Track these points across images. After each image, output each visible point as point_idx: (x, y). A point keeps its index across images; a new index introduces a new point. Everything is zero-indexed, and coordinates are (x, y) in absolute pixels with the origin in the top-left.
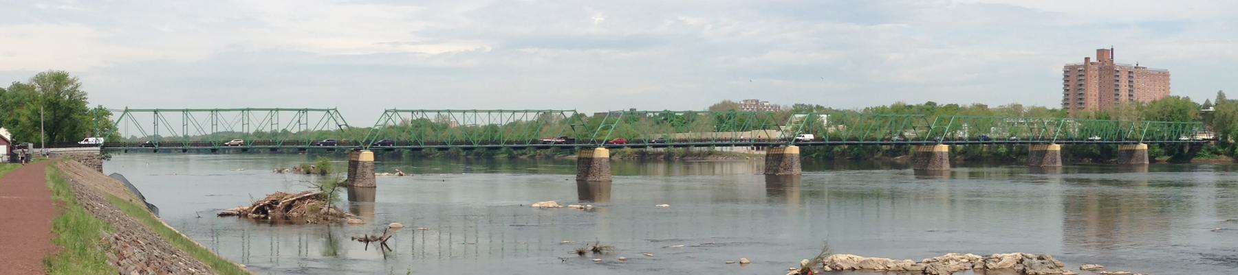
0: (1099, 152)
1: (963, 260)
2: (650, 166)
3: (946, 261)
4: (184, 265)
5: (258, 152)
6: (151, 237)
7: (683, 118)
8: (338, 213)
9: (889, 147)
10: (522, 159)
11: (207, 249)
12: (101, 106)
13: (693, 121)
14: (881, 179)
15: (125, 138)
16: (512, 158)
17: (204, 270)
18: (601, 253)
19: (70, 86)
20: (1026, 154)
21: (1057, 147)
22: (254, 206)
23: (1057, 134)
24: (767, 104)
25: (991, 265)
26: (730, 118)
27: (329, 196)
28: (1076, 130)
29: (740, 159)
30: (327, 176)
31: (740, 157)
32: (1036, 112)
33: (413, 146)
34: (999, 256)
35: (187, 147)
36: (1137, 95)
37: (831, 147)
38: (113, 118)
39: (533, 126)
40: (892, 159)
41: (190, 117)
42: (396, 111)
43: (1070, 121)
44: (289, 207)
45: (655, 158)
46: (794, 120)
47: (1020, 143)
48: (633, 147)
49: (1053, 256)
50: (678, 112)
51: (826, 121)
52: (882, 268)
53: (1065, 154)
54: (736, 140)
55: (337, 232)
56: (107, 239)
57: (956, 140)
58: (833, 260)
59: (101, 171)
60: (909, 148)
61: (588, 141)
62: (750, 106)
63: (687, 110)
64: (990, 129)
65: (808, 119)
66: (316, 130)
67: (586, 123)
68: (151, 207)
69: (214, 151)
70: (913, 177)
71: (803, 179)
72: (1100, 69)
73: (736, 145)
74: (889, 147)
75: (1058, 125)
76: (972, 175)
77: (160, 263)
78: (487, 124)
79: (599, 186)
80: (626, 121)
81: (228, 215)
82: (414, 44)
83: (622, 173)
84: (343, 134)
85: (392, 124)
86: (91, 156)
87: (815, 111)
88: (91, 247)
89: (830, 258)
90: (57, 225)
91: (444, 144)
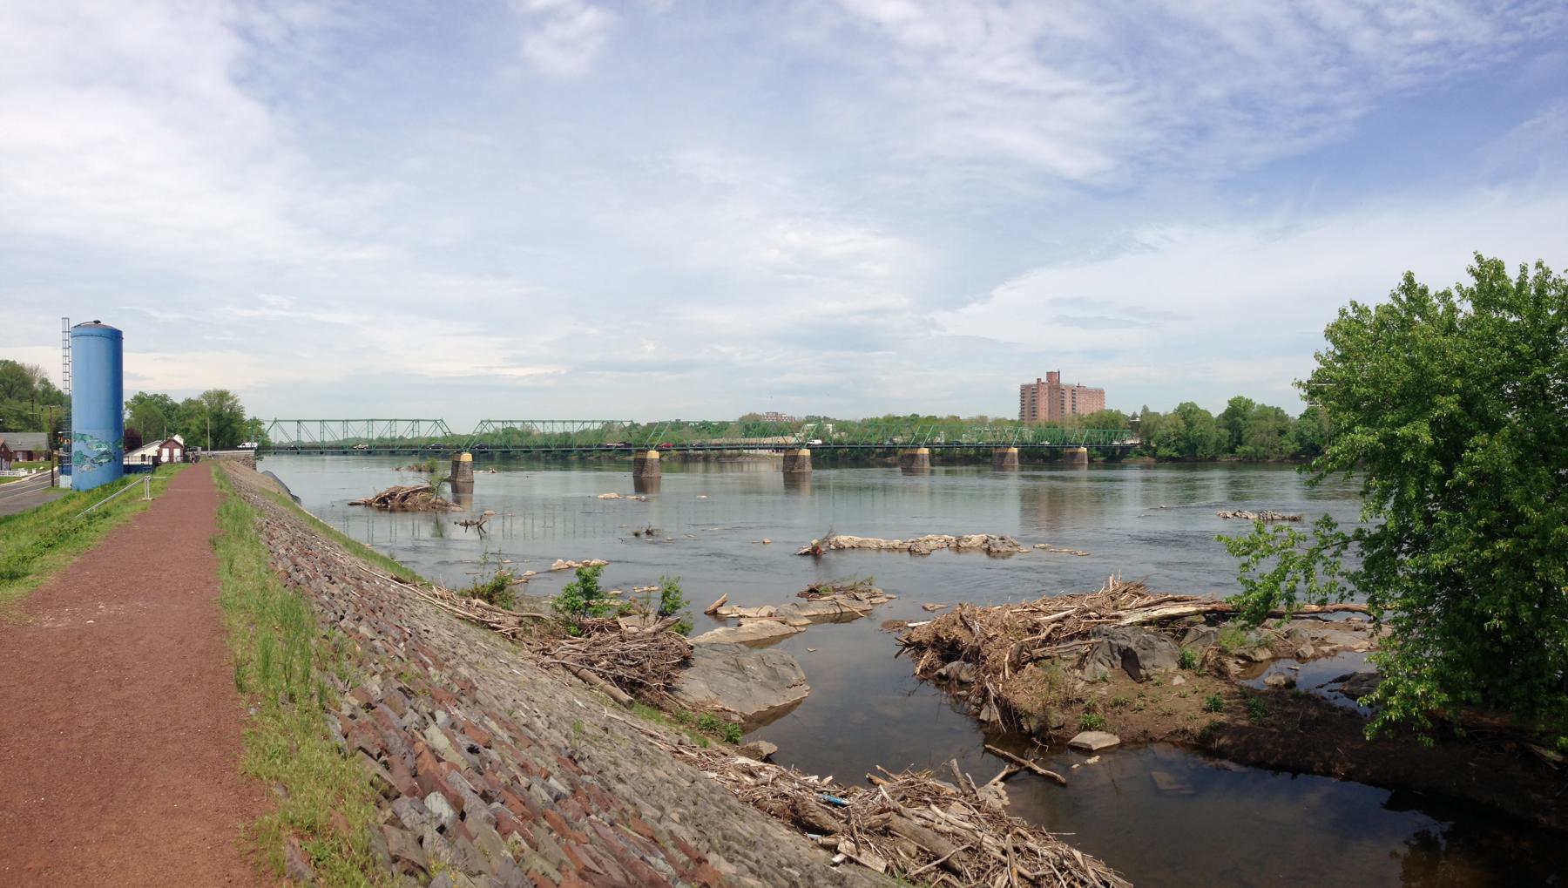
2: (691, 465)
7: (718, 427)
9: (881, 450)
14: (875, 475)
16: (582, 459)
21: (1015, 450)
25: (963, 544)
32: (999, 422)
34: (969, 537)
36: (1078, 407)
38: (265, 427)
39: (598, 433)
42: (489, 421)
43: (1026, 429)
44: (404, 498)
45: (695, 459)
53: (1021, 456)
55: (443, 518)
56: (260, 524)
59: (255, 469)
68: (295, 498)
69: (345, 453)
70: (900, 474)
71: (813, 475)
72: (1049, 388)
74: (881, 450)
76: (947, 472)
78: (562, 432)
81: (356, 504)
82: (503, 367)
83: (669, 471)
86: (247, 457)
89: (834, 539)
91: (528, 447)
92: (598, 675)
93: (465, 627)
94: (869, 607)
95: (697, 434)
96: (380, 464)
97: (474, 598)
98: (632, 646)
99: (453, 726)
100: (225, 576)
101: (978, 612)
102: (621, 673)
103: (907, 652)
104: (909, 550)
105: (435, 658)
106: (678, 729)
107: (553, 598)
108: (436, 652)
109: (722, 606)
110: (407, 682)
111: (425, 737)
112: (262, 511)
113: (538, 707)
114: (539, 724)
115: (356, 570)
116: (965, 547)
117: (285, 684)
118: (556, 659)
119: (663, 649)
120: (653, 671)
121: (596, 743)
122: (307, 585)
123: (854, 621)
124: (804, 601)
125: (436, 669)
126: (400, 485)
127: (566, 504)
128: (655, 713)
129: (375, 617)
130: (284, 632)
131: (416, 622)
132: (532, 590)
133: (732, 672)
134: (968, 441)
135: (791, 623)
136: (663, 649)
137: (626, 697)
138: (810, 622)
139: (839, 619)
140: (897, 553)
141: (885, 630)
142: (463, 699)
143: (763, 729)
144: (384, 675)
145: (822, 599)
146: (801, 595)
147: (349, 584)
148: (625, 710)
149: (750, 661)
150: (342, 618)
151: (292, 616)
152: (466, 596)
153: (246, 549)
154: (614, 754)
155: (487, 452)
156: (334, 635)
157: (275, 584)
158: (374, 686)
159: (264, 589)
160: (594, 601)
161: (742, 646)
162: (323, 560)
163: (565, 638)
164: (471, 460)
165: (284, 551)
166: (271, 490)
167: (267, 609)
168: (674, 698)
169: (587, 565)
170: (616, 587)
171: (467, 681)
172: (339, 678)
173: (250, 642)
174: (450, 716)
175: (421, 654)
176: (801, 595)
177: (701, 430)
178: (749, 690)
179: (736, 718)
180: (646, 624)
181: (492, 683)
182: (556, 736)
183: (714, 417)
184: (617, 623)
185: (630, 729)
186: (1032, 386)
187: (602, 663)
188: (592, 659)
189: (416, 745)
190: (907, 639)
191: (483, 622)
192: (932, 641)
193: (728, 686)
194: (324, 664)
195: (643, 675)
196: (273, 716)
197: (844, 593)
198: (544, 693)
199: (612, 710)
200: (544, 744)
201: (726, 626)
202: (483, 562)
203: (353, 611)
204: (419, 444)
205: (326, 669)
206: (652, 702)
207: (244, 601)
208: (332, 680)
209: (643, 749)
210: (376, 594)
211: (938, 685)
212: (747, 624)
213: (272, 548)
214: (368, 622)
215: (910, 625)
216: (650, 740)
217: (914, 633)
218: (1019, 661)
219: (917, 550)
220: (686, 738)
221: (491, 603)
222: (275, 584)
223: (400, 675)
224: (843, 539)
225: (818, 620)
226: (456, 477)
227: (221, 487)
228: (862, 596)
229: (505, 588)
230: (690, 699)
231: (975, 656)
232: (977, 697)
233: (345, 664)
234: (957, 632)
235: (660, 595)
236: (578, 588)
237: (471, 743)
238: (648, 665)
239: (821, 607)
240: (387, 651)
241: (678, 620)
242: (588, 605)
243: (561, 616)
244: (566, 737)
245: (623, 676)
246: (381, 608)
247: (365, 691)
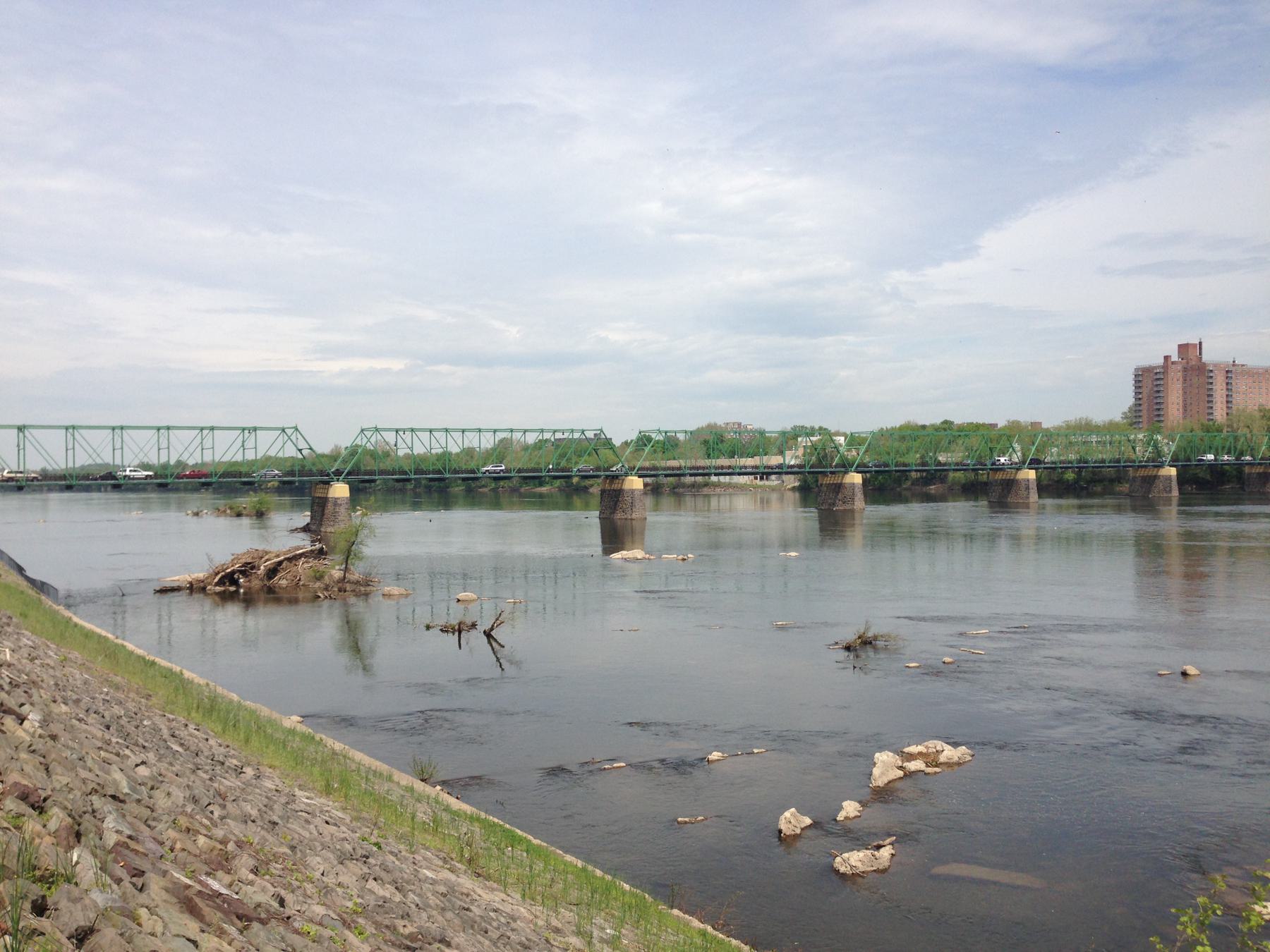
0: (1208, 477)
10: (480, 492)
16: (469, 491)
21: (1032, 474)
29: (742, 490)
31: (742, 488)
33: (430, 476)
36: (1238, 399)
40: (924, 489)
41: (30, 437)
42: (377, 430)
44: (273, 572)
47: (1093, 467)
53: (1182, 480)
71: (866, 513)
72: (1185, 370)
78: (200, 462)
81: (173, 590)
126: (260, 548)
186: (1155, 368)
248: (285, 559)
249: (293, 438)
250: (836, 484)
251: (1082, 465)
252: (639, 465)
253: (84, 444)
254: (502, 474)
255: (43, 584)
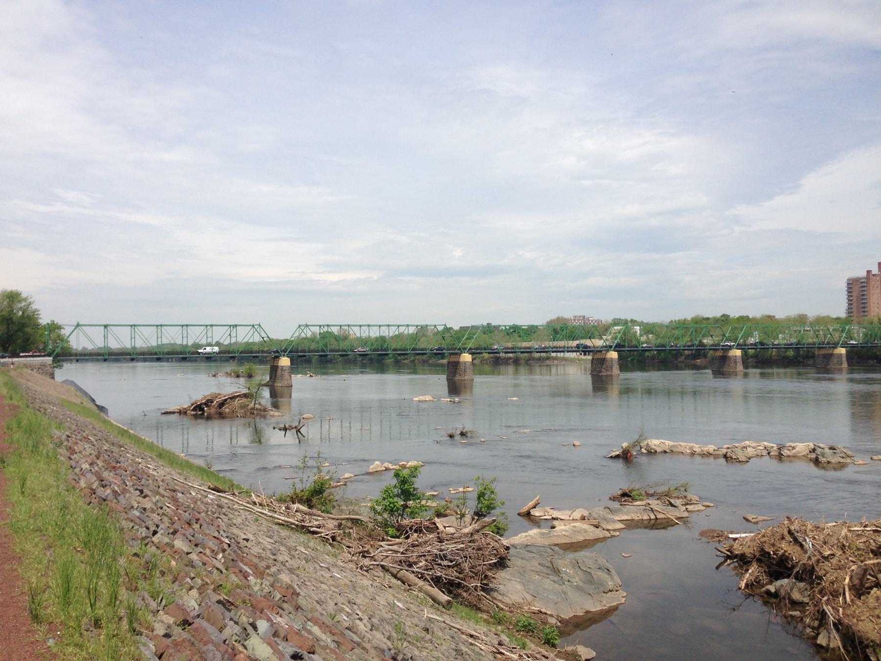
1: (760, 448)
2: (502, 368)
3: (744, 447)
4: (132, 457)
5: (196, 361)
6: (100, 434)
7: (527, 330)
8: (262, 408)
9: (690, 352)
11: (152, 442)
12: (53, 321)
13: (534, 333)
14: (685, 378)
15: (77, 349)
16: (397, 362)
17: (149, 460)
18: (467, 437)
19: (23, 304)
20: (813, 356)
21: (843, 351)
22: (192, 405)
23: (842, 339)
24: (592, 319)
25: (785, 452)
26: (563, 330)
27: (255, 394)
28: (861, 335)
30: (253, 379)
32: (821, 321)
33: (341, 353)
34: (793, 445)
35: (134, 357)
37: (643, 352)
38: (65, 332)
39: (414, 338)
40: (693, 362)
42: (307, 326)
43: (855, 328)
44: (222, 405)
45: (506, 361)
46: (613, 331)
47: (807, 348)
48: (489, 353)
49: (844, 447)
50: (524, 326)
51: (639, 332)
52: (689, 451)
54: (568, 348)
55: (261, 424)
56: (59, 438)
57: (748, 346)
58: (648, 444)
59: (53, 378)
60: (708, 353)
61: (455, 349)
62: (579, 321)
63: (530, 324)
64: (778, 336)
65: (624, 331)
66: (243, 342)
67: (454, 336)
68: (102, 409)
69: (159, 360)
70: (711, 376)
73: (568, 352)
74: (690, 352)
75: (842, 331)
76: (763, 375)
77: (109, 456)
78: (378, 335)
79: (464, 384)
80: (484, 333)
82: (317, 273)
83: (481, 373)
84: (265, 345)
85: (304, 336)
86: (44, 365)
87: (629, 324)
88: (43, 444)
89: (646, 442)
90: (10, 427)
91: (345, 351)
92: (417, 576)
93: (285, 533)
94: (686, 514)
95: (507, 337)
96: (196, 371)
97: (294, 503)
98: (449, 547)
99: (276, 634)
100: (16, 497)
101: (809, 527)
102: (439, 574)
103: (729, 565)
104: (725, 456)
105: (255, 567)
106: (496, 630)
107: (371, 500)
108: (256, 560)
109: (535, 507)
110: (226, 595)
111: (246, 648)
112: (60, 424)
113: (360, 610)
114: (361, 626)
115: (170, 481)
116: (789, 456)
117: (89, 610)
118: (375, 561)
119: (480, 549)
120: (471, 571)
121: (418, 644)
122: (115, 501)
123: (669, 528)
124: (616, 505)
125: (256, 577)
127: (382, 405)
128: (473, 613)
129: (191, 530)
130: (87, 553)
131: (235, 531)
132: (351, 492)
133: (547, 574)
134: (786, 341)
135: (604, 527)
136: (480, 549)
137: (444, 598)
138: (624, 527)
139: (656, 525)
140: (711, 459)
141: (704, 539)
142: (285, 606)
143: (579, 633)
144: (202, 589)
145: (635, 504)
146: (613, 499)
147: (163, 496)
148: (444, 610)
149: (564, 563)
150: (155, 533)
151: (98, 535)
152: (285, 501)
153: (42, 465)
154: (435, 654)
155: (304, 356)
156: (145, 552)
157: (76, 503)
158: (191, 601)
159: (64, 508)
160: (411, 502)
161: (557, 548)
162: (133, 474)
163: (383, 540)
164: (289, 364)
165: (88, 466)
166: (73, 400)
167: (67, 529)
168: (491, 599)
169: (404, 467)
170: (432, 488)
171: (289, 587)
172: (152, 597)
173: (48, 567)
174: (272, 624)
175: (241, 565)
176: (613, 499)
177: (512, 333)
178: (565, 593)
179: (553, 621)
180: (462, 524)
181: (313, 588)
182: (379, 638)
183: (523, 321)
184: (435, 524)
185: (450, 629)
187: (421, 564)
188: (411, 560)
189: (237, 657)
190: (728, 551)
191: (303, 527)
192: (757, 554)
193: (545, 589)
194: (134, 584)
195: (461, 576)
196: (76, 645)
197: (658, 499)
198: (365, 595)
199: (432, 610)
200: (368, 646)
201: (539, 527)
202: (302, 465)
203: (168, 525)
204: (236, 349)
205: (136, 589)
206: (470, 603)
207: (39, 523)
208: (143, 599)
209: (464, 649)
210: (192, 506)
211: (766, 603)
212: (560, 527)
213: (73, 463)
214: (184, 535)
215: (731, 536)
216: (471, 640)
217: (736, 545)
218: (862, 584)
219: (734, 457)
220: (504, 638)
221: (310, 507)
222: (76, 503)
223: (218, 588)
224: (655, 443)
225: (631, 525)
226: (274, 382)
227: (11, 399)
228: (678, 502)
229: (324, 491)
230: (507, 600)
231: (808, 575)
232: (813, 620)
233: (158, 581)
234: (786, 547)
235: (476, 496)
236: (395, 490)
237: (295, 649)
238: (466, 566)
239: (634, 511)
240: (204, 564)
241: (494, 521)
242: (405, 507)
243: (379, 518)
244: (389, 638)
245: (441, 577)
246: (198, 520)
247: (182, 609)
248: (229, 398)
249: (258, 330)
250: (829, 354)
251: (799, 346)
252: (469, 346)
253: (140, 334)
254: (646, 348)
255: (102, 407)
